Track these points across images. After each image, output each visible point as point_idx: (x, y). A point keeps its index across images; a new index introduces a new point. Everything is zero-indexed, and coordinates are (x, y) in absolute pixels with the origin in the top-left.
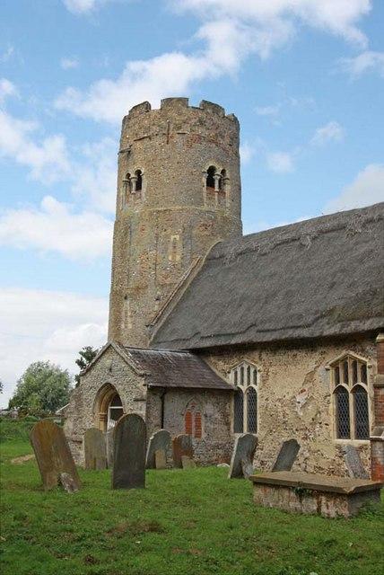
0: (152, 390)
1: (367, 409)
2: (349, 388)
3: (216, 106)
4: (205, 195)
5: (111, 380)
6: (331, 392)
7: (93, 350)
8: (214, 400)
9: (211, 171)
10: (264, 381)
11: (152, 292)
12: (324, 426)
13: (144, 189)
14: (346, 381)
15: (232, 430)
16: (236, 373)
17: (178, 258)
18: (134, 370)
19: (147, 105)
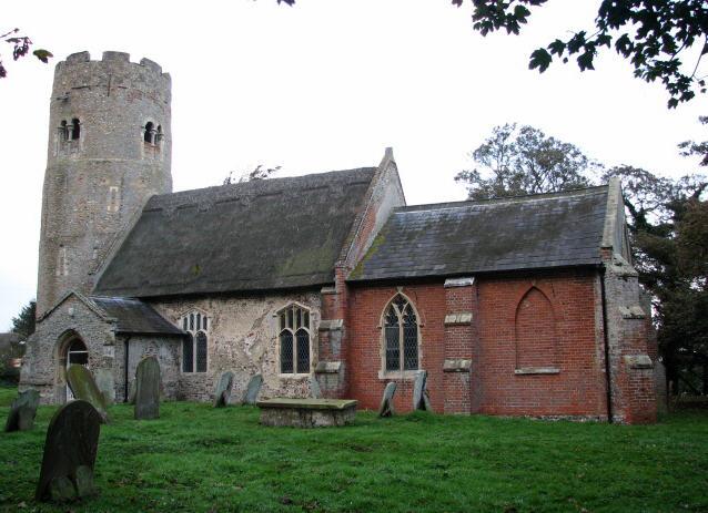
0: (118, 335)
2: (294, 332)
5: (73, 326)
8: (167, 344)
9: (149, 126)
10: (214, 327)
11: (90, 241)
13: (82, 138)
14: (291, 326)
15: (182, 370)
16: (186, 319)
17: (117, 208)
19: (85, 55)
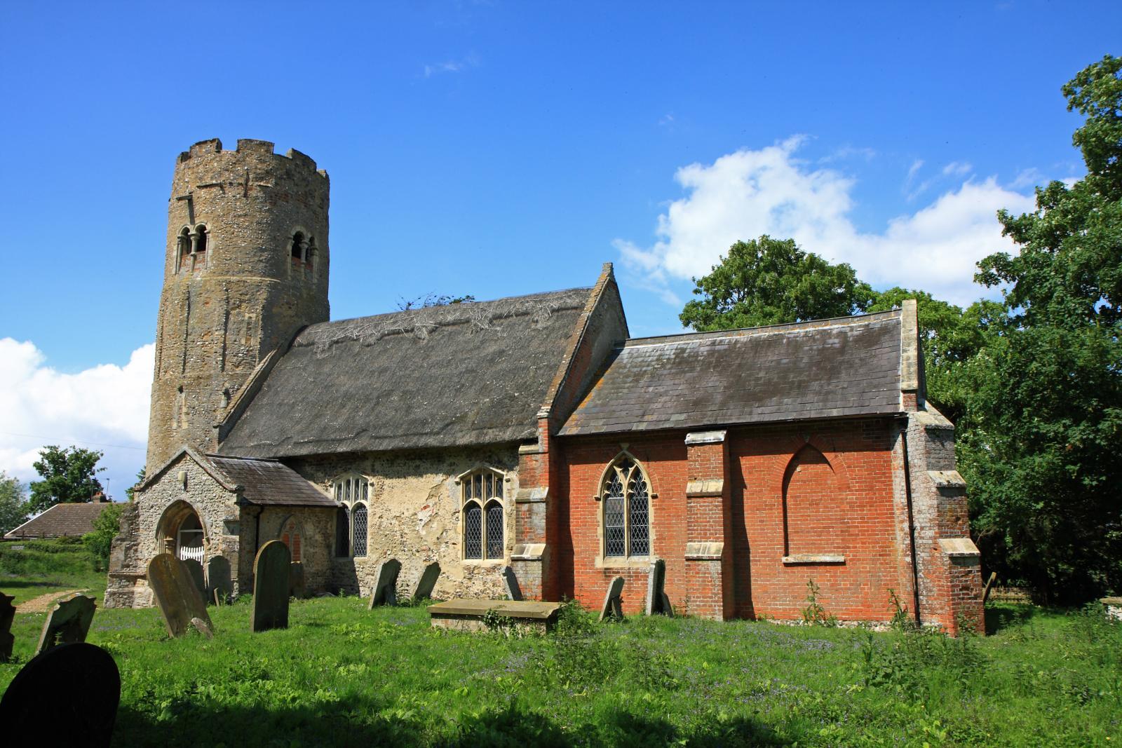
1: (501, 525)
3: (307, 157)
4: (289, 266)
5: (185, 496)
6: (461, 508)
7: (60, 450)
9: (298, 237)
12: (451, 546)
18: (221, 484)
